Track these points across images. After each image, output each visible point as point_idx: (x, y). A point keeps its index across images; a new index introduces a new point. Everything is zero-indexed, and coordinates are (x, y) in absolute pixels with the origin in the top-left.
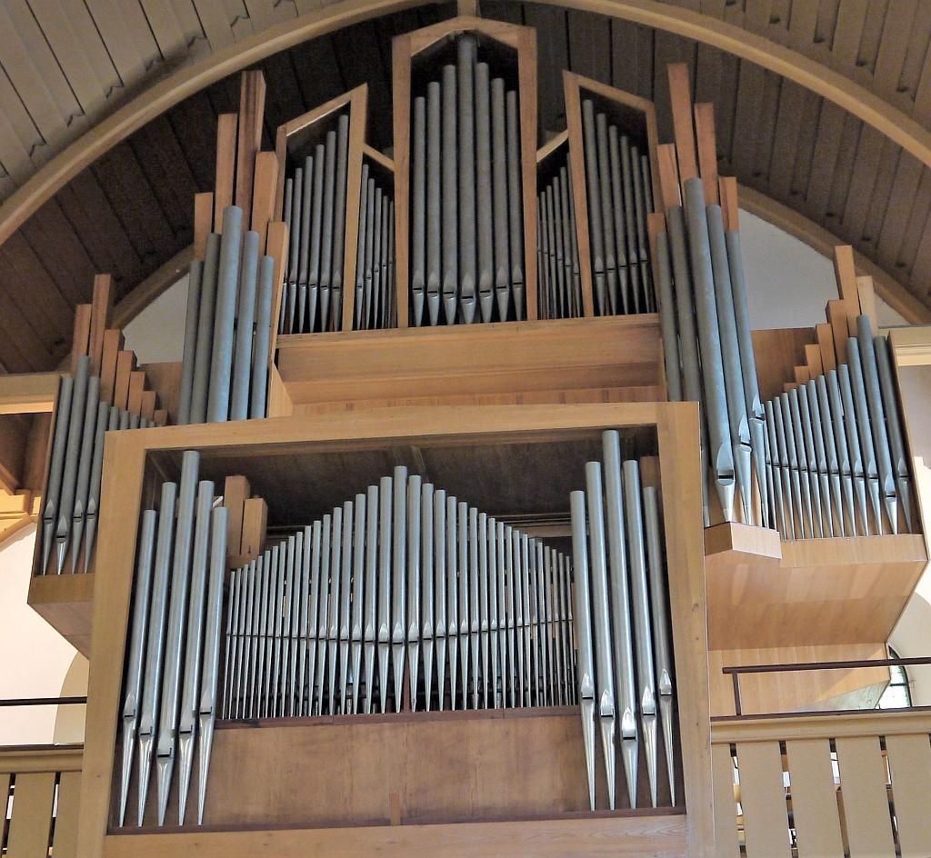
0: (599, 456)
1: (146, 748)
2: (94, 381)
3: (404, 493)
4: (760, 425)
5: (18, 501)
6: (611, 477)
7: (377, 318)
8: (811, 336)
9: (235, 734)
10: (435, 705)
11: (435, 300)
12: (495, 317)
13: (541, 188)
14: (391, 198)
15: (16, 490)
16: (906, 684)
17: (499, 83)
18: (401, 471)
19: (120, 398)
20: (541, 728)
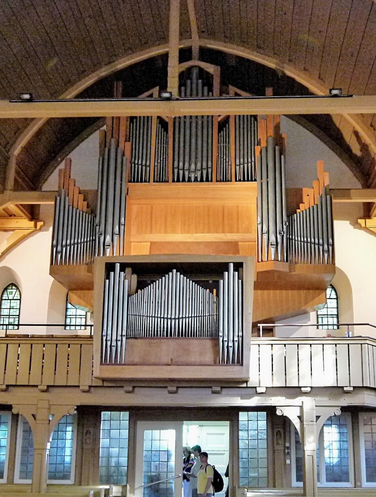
0: (228, 270)
2: (67, 198)
6: (231, 275)
7: (161, 179)
10: (182, 336)
11: (181, 172)
13: (219, 132)
14: (167, 133)
15: (31, 220)
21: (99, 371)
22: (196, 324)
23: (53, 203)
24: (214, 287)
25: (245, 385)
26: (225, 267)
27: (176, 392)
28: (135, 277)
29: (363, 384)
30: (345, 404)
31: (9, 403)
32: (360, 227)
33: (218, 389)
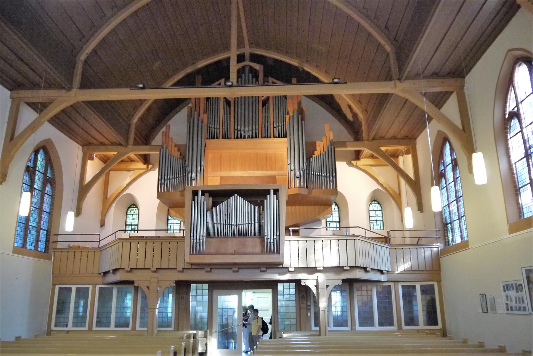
1: (195, 241)
3: (237, 199)
5: (145, 166)
6: (271, 197)
7: (226, 137)
9: (209, 239)
11: (239, 132)
13: (263, 106)
14: (230, 107)
15: (145, 164)
16: (339, 211)
17: (254, 79)
21: (189, 259)
22: (250, 228)
23: (158, 153)
24: (261, 205)
25: (281, 266)
26: (267, 192)
27: (238, 271)
31: (132, 280)
33: (265, 269)
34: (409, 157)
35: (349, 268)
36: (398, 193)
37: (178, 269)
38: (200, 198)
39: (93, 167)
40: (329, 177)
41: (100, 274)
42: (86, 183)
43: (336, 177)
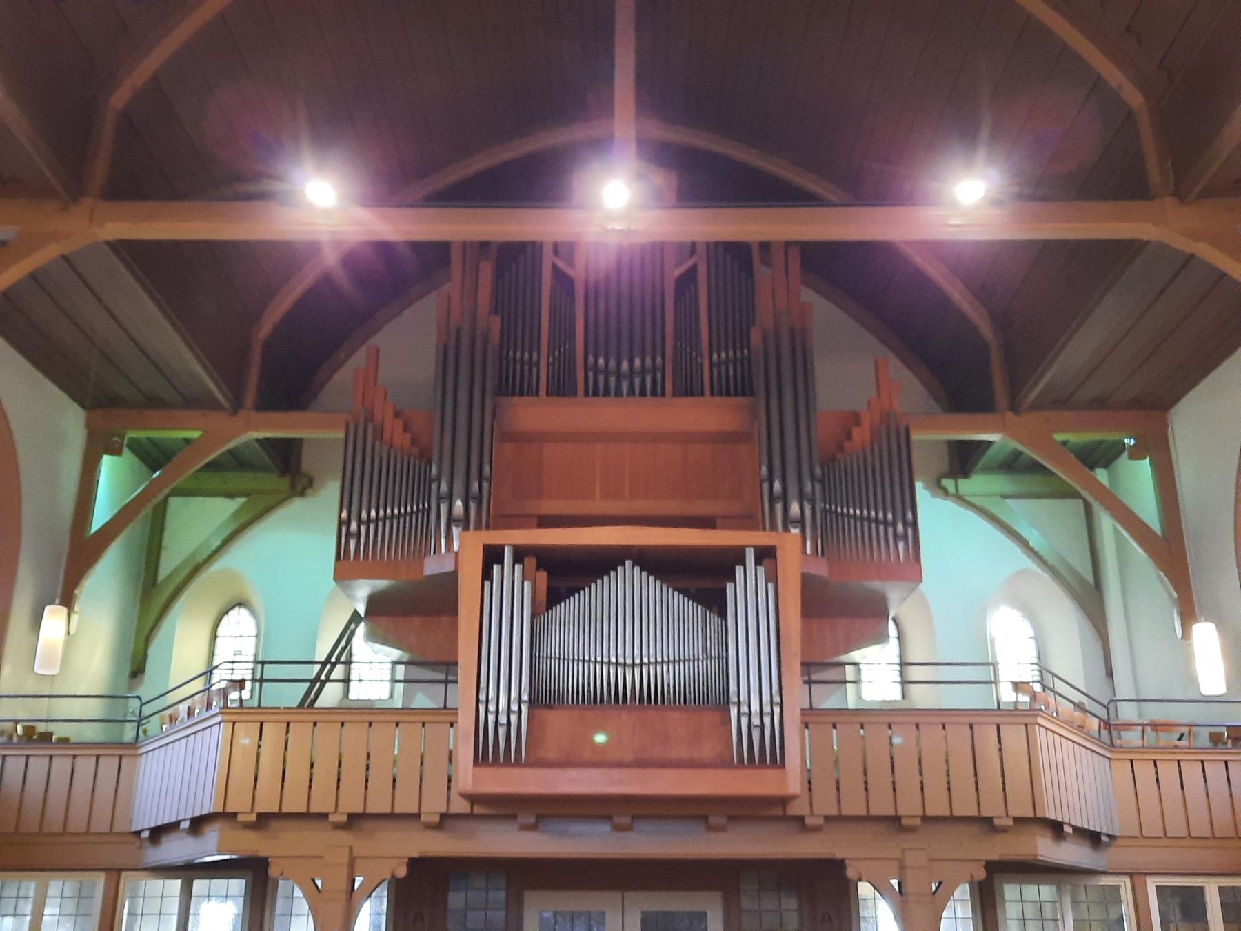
3: (629, 573)
4: (818, 486)
7: (562, 388)
8: (856, 418)
12: (643, 393)
18: (628, 563)
19: (387, 435)
20: (709, 718)
21: (468, 777)
23: (341, 435)
24: (714, 602)
25: (778, 811)
27: (628, 828)
28: (543, 576)
29: (840, 808)
30: (995, 857)
31: (262, 854)
32: (946, 493)
33: (626, 820)
34: (1144, 467)
35: (1011, 823)
36: (1089, 577)
37: (423, 818)
38: (509, 572)
39: (113, 480)
40: (894, 525)
41: (138, 833)
42: (93, 531)
43: (915, 525)
